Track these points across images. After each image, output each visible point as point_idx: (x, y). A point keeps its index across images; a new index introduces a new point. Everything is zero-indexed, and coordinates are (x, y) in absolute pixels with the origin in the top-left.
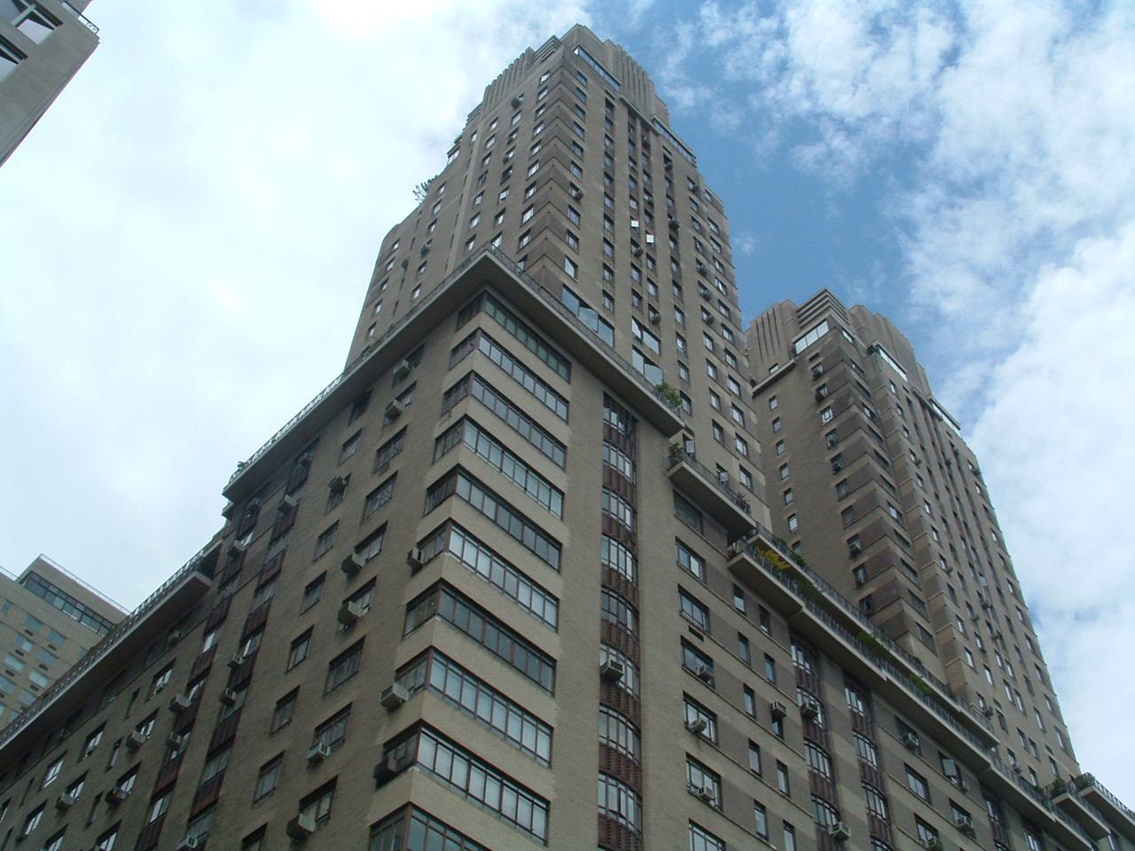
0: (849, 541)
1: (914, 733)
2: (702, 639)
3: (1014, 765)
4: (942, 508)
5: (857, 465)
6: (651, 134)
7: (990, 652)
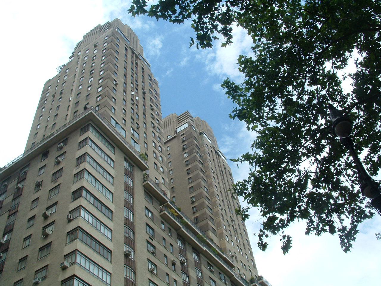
0: (191, 198)
1: (212, 266)
2: (152, 240)
3: (239, 273)
4: (220, 187)
5: (195, 173)
6: (138, 59)
7: (233, 236)
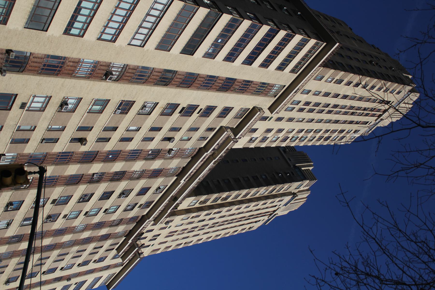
2: (198, 113)
